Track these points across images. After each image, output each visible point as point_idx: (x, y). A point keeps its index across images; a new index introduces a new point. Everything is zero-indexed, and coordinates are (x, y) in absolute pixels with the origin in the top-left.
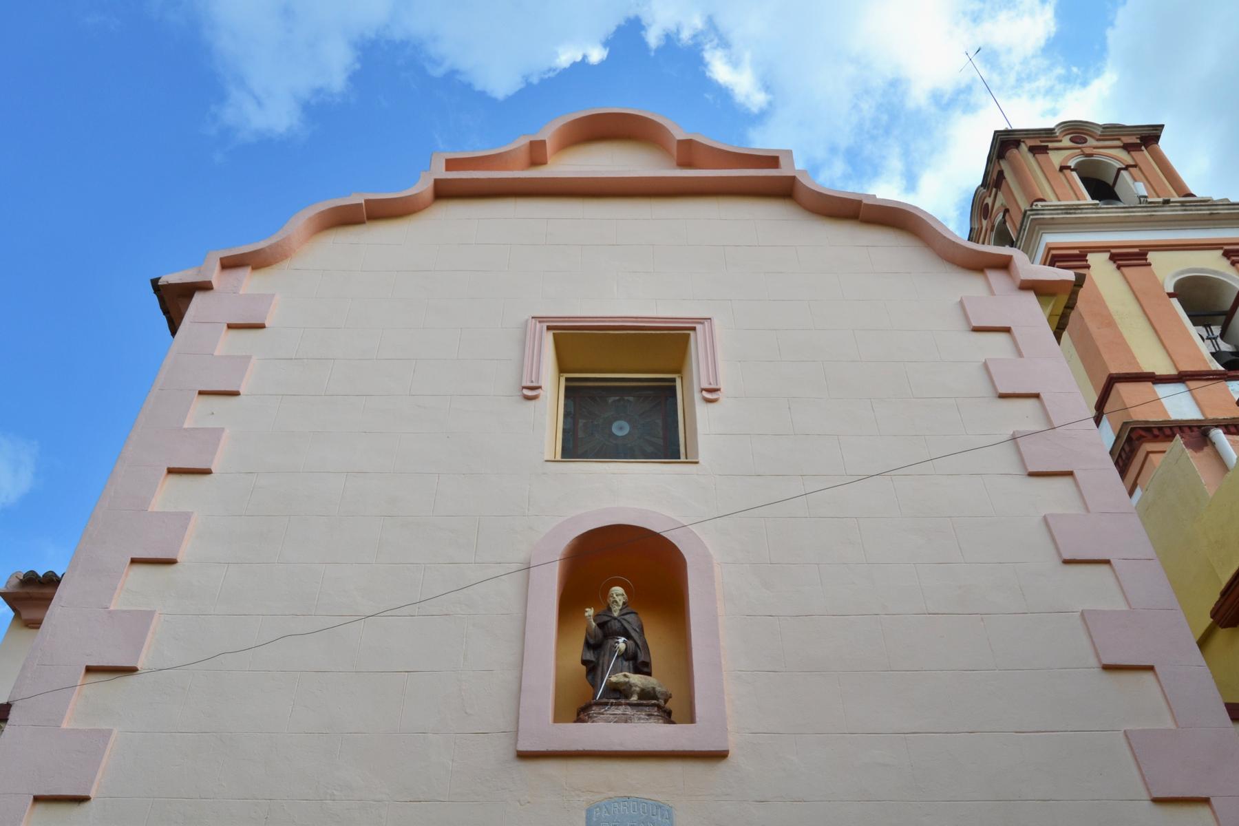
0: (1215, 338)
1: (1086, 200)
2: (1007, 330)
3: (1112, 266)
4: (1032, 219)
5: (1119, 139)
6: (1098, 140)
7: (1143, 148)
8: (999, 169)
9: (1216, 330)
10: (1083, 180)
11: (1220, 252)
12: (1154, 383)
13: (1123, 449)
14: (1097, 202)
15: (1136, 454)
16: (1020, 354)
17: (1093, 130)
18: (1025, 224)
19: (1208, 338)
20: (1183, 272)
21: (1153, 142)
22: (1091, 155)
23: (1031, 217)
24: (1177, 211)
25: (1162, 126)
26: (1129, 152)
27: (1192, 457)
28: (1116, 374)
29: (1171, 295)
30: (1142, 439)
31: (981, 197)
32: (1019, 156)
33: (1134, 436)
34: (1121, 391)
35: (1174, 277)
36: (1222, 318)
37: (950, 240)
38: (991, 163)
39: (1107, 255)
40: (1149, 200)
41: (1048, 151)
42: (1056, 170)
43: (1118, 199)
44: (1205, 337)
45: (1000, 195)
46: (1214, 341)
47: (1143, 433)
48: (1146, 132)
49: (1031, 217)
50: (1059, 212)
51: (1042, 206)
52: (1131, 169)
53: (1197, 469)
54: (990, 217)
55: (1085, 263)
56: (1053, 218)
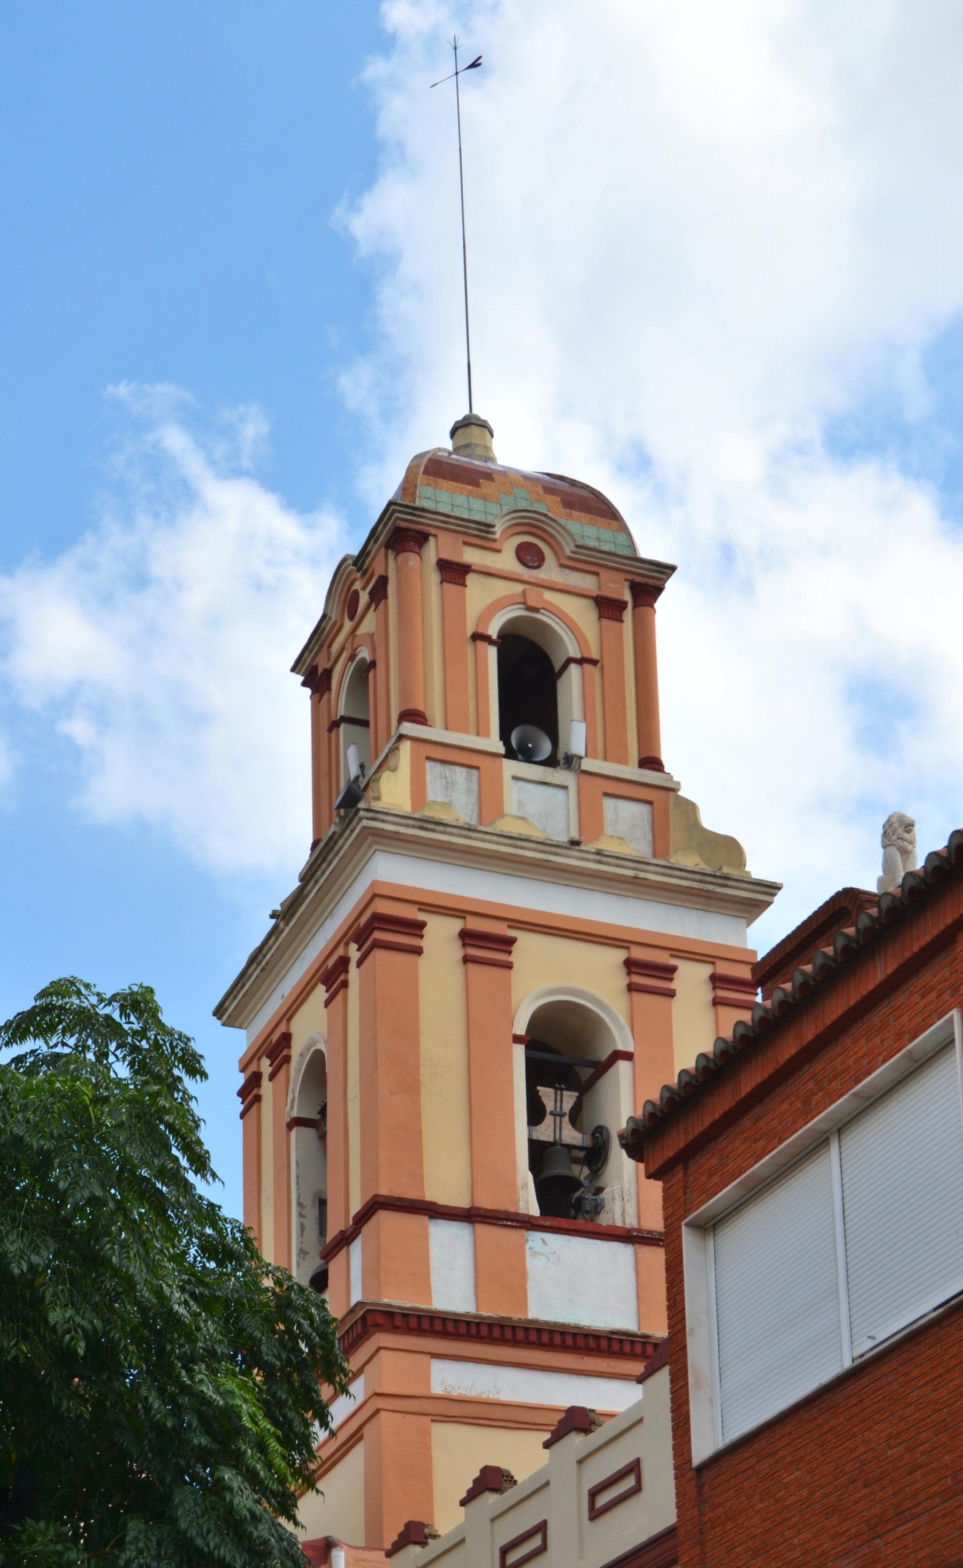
0: (562, 1115)
4: (364, 828)
11: (618, 956)
12: (431, 1217)
15: (368, 1339)
17: (559, 537)
19: (551, 1113)
20: (552, 992)
23: (365, 823)
24: (587, 860)
25: (673, 569)
29: (517, 1039)
30: (379, 1327)
35: (537, 999)
38: (376, 541)
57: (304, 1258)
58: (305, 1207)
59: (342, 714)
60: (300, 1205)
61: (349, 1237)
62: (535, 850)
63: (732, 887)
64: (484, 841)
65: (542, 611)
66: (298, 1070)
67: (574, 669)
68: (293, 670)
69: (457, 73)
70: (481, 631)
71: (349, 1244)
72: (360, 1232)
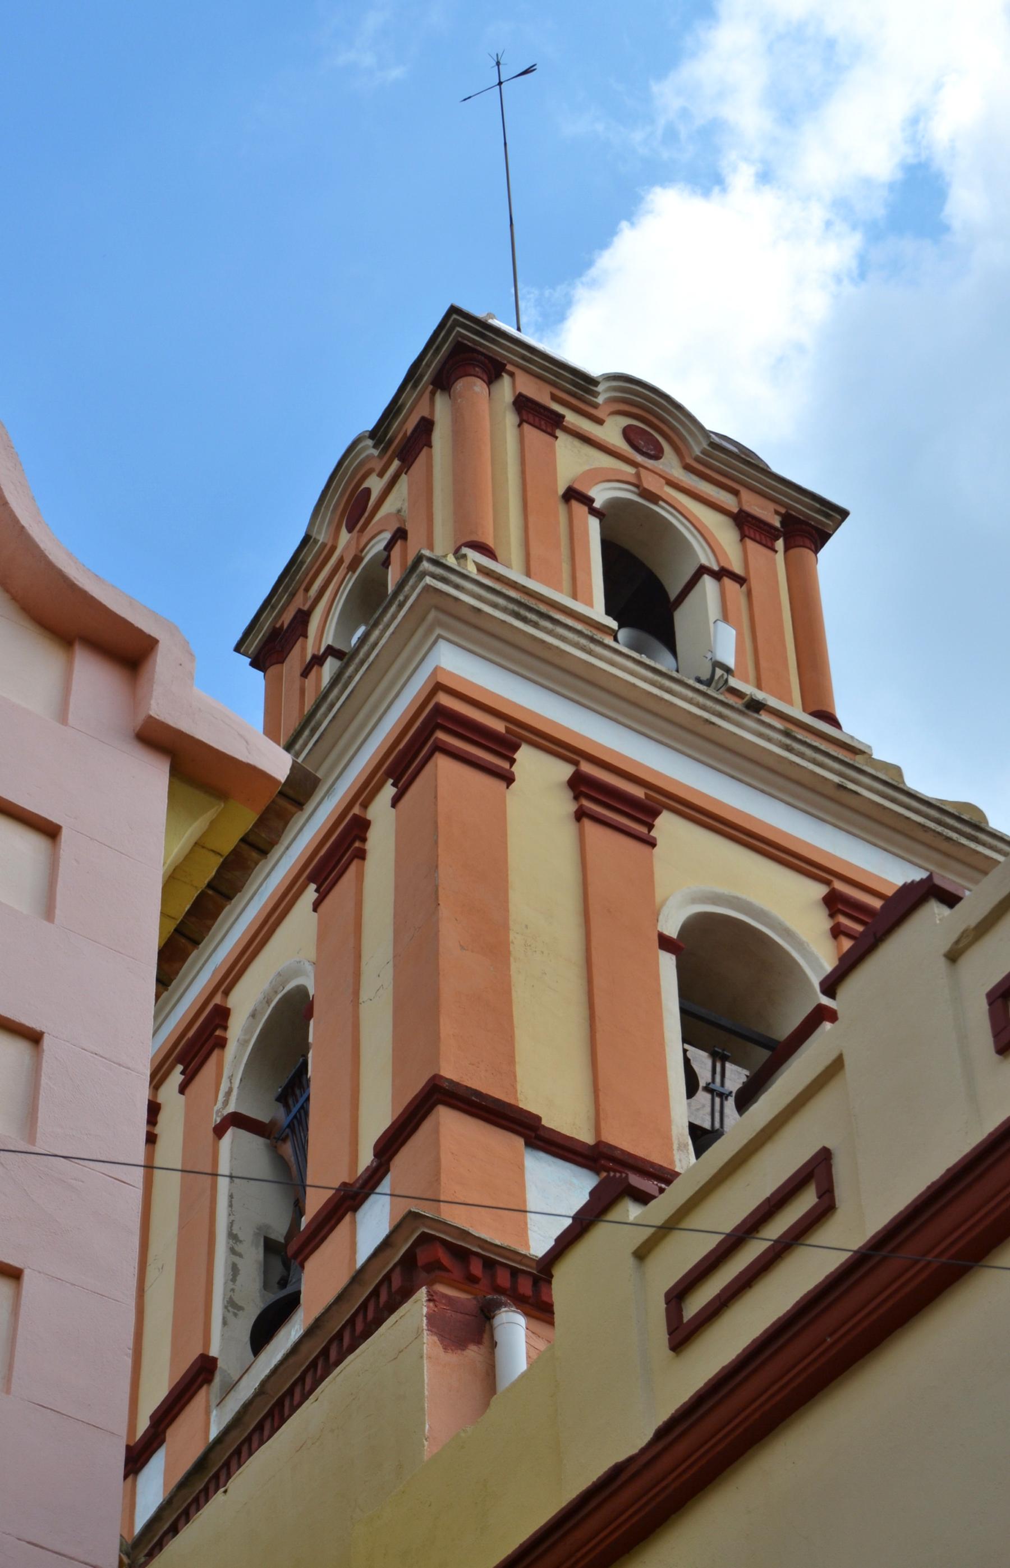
0: (723, 1096)
1: (590, 603)
2: (50, 831)
3: (565, 805)
4: (428, 588)
5: (736, 493)
6: (687, 468)
7: (780, 544)
8: (426, 414)
9: (735, 1077)
10: (607, 546)
11: (820, 890)
13: (387, 1278)
14: (614, 624)
16: (49, 913)
18: (407, 588)
19: (707, 1089)
20: (716, 899)
21: (808, 542)
22: (654, 498)
23: (428, 580)
24: (769, 740)
25: (844, 514)
26: (743, 537)
27: (429, 1358)
28: (451, 1081)
29: (665, 943)
31: (361, 464)
32: (483, 405)
33: (423, 1257)
34: (443, 1130)
35: (694, 900)
36: (763, 1055)
37: (16, 521)
39: (566, 771)
40: (734, 682)
41: (558, 433)
42: (556, 492)
43: (670, 642)
44: (702, 1083)
45: (403, 483)
46: (717, 1100)
47: (445, 1259)
48: (802, 508)
49: (428, 580)
50: (501, 602)
51: (481, 569)
52: (727, 581)
53: (426, 1393)
54: (362, 530)
55: (506, 765)
56: (479, 611)
57: (235, 1315)
58: (241, 1242)
59: (330, 642)
60: (232, 1236)
61: (357, 1194)
62: (690, 701)
63: (984, 844)
64: (613, 664)
65: (661, 503)
66: (244, 1043)
67: (708, 584)
68: (237, 649)
69: (500, 83)
70: (578, 486)
71: (355, 1208)
72: (387, 1171)
